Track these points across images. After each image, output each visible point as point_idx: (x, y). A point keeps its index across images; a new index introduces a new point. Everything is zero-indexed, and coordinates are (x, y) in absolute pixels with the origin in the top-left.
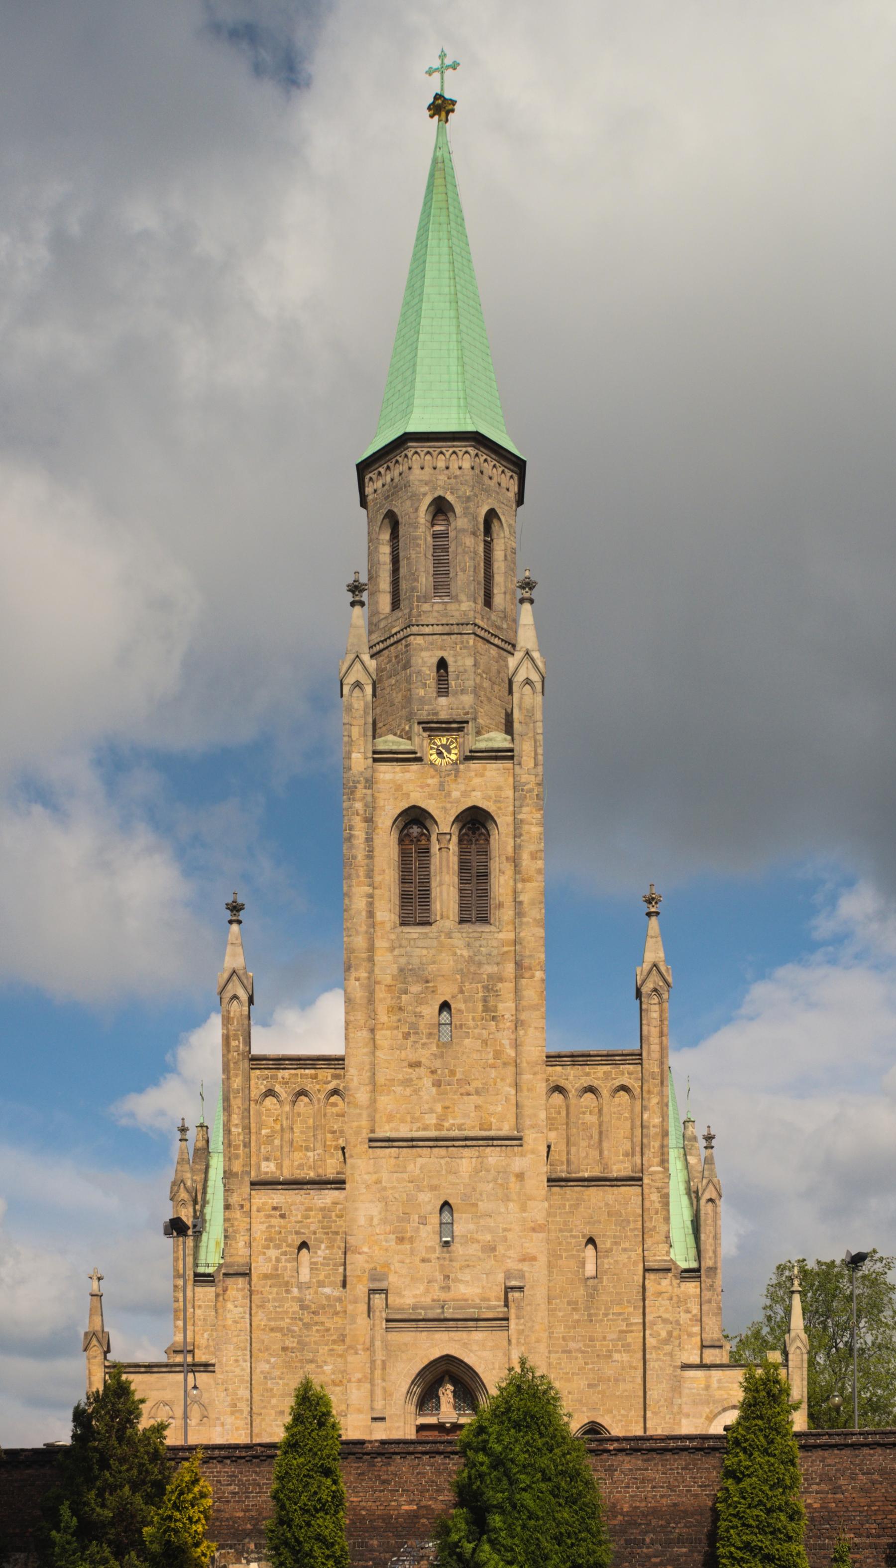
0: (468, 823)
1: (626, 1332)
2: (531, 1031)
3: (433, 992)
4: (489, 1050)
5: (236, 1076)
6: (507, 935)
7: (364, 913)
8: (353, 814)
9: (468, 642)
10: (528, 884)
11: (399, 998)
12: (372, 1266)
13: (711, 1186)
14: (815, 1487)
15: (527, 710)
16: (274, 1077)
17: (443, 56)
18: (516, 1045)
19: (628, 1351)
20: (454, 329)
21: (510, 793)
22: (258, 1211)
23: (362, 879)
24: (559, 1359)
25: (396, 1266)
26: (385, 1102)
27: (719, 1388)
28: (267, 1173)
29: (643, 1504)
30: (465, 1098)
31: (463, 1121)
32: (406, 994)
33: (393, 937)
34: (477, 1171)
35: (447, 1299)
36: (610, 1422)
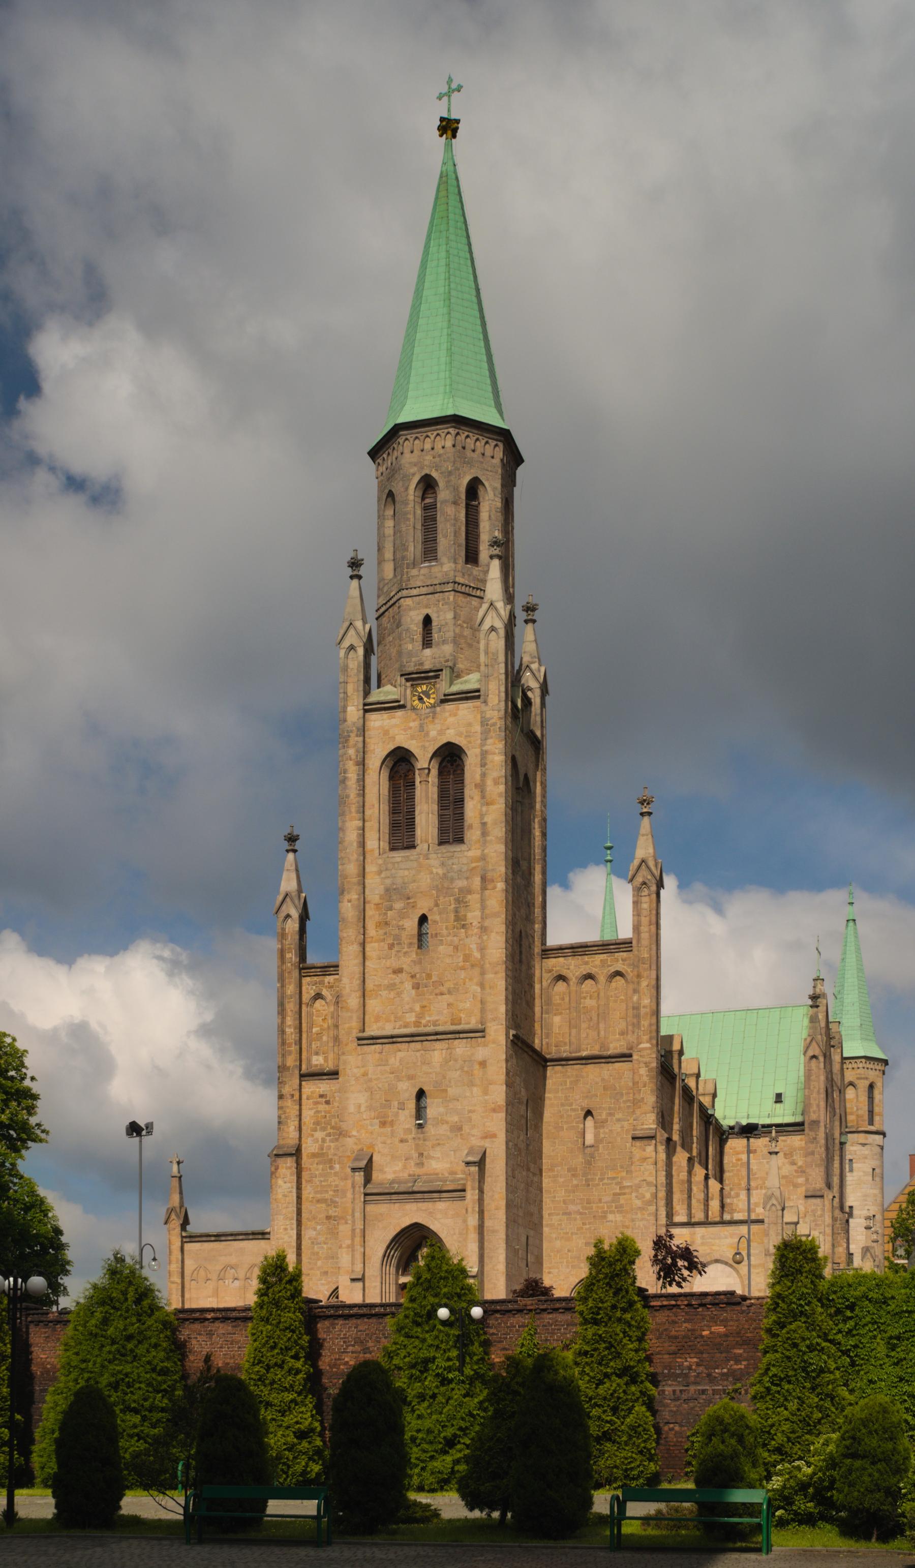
0: (447, 756)
1: (620, 1194)
2: (493, 935)
5: (290, 984)
6: (474, 853)
7: (355, 844)
8: (347, 759)
9: (449, 599)
10: (491, 806)
11: (386, 914)
12: (359, 1147)
13: (814, 1043)
14: (350, 1349)
15: (493, 654)
16: (322, 982)
17: (450, 81)
18: (482, 949)
19: (620, 1212)
20: (445, 324)
21: (477, 728)
22: (308, 1099)
23: (354, 814)
24: (560, 1220)
25: (379, 1147)
26: (373, 1005)
27: (703, 1244)
28: (316, 1065)
29: (232, 1361)
30: (439, 997)
31: (437, 1018)
32: (391, 910)
33: (380, 861)
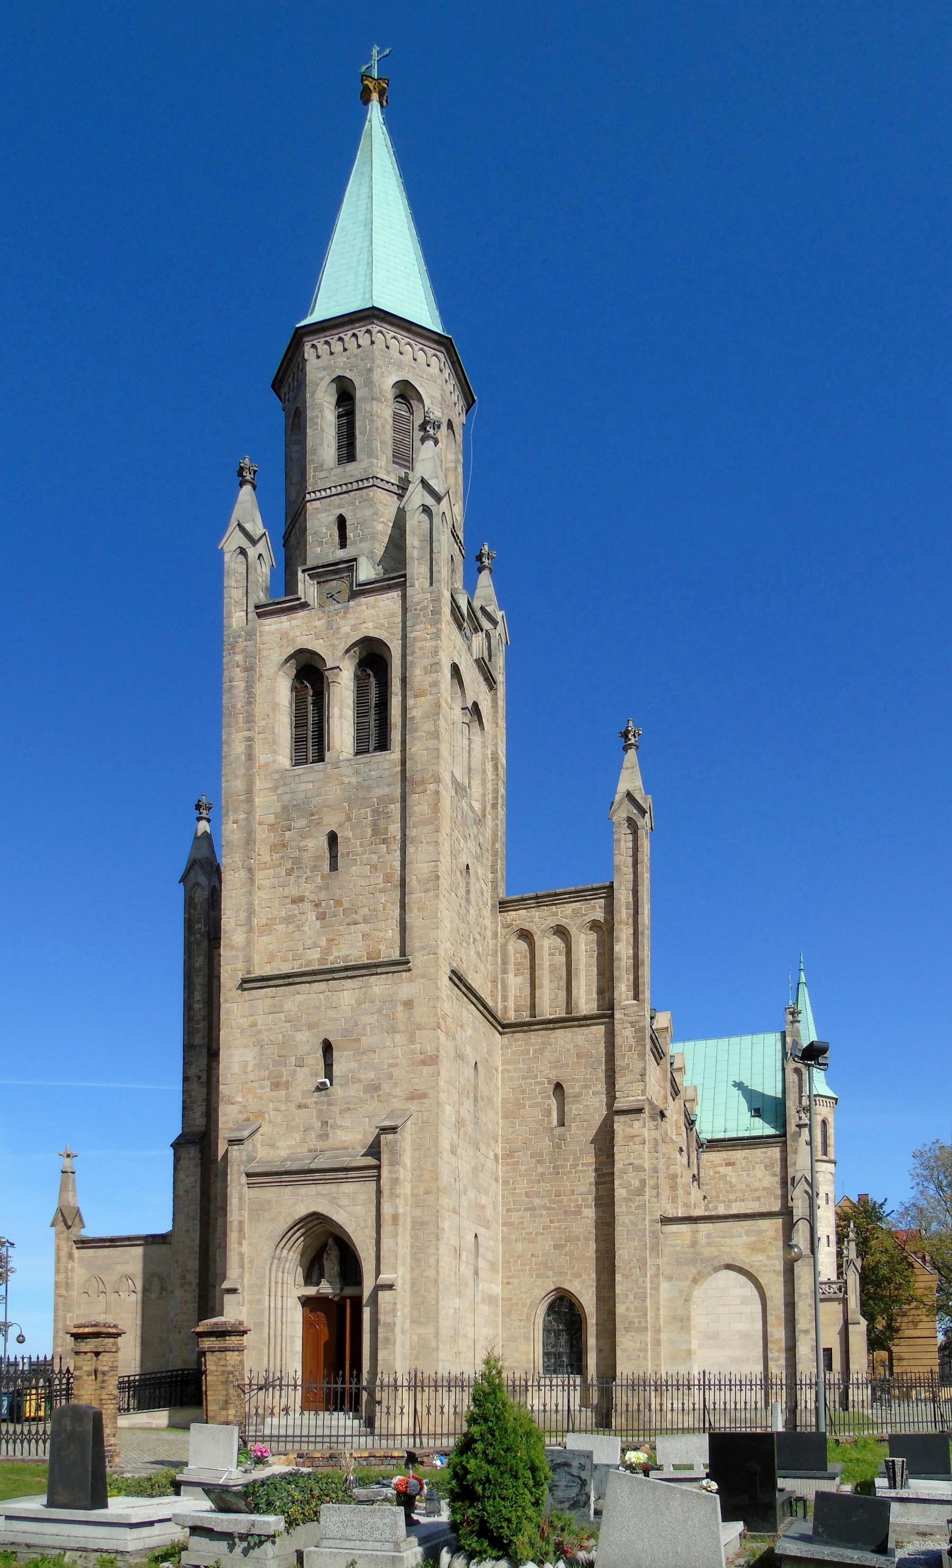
3: (318, 823)
4: (377, 874)
7: (243, 757)
12: (245, 1116)
23: (241, 725)
24: (522, 1217)
31: (349, 952)
34: (360, 1003)
35: (324, 1148)
36: (579, 1288)
